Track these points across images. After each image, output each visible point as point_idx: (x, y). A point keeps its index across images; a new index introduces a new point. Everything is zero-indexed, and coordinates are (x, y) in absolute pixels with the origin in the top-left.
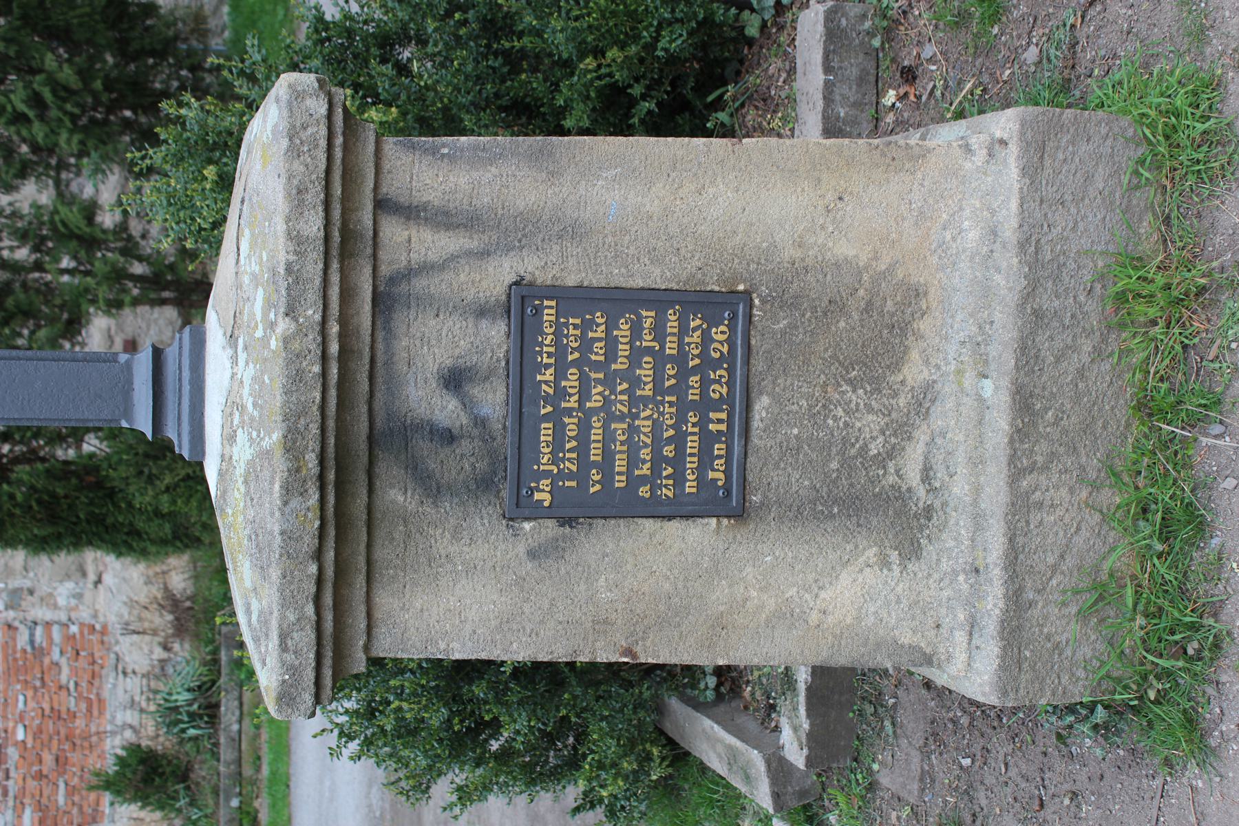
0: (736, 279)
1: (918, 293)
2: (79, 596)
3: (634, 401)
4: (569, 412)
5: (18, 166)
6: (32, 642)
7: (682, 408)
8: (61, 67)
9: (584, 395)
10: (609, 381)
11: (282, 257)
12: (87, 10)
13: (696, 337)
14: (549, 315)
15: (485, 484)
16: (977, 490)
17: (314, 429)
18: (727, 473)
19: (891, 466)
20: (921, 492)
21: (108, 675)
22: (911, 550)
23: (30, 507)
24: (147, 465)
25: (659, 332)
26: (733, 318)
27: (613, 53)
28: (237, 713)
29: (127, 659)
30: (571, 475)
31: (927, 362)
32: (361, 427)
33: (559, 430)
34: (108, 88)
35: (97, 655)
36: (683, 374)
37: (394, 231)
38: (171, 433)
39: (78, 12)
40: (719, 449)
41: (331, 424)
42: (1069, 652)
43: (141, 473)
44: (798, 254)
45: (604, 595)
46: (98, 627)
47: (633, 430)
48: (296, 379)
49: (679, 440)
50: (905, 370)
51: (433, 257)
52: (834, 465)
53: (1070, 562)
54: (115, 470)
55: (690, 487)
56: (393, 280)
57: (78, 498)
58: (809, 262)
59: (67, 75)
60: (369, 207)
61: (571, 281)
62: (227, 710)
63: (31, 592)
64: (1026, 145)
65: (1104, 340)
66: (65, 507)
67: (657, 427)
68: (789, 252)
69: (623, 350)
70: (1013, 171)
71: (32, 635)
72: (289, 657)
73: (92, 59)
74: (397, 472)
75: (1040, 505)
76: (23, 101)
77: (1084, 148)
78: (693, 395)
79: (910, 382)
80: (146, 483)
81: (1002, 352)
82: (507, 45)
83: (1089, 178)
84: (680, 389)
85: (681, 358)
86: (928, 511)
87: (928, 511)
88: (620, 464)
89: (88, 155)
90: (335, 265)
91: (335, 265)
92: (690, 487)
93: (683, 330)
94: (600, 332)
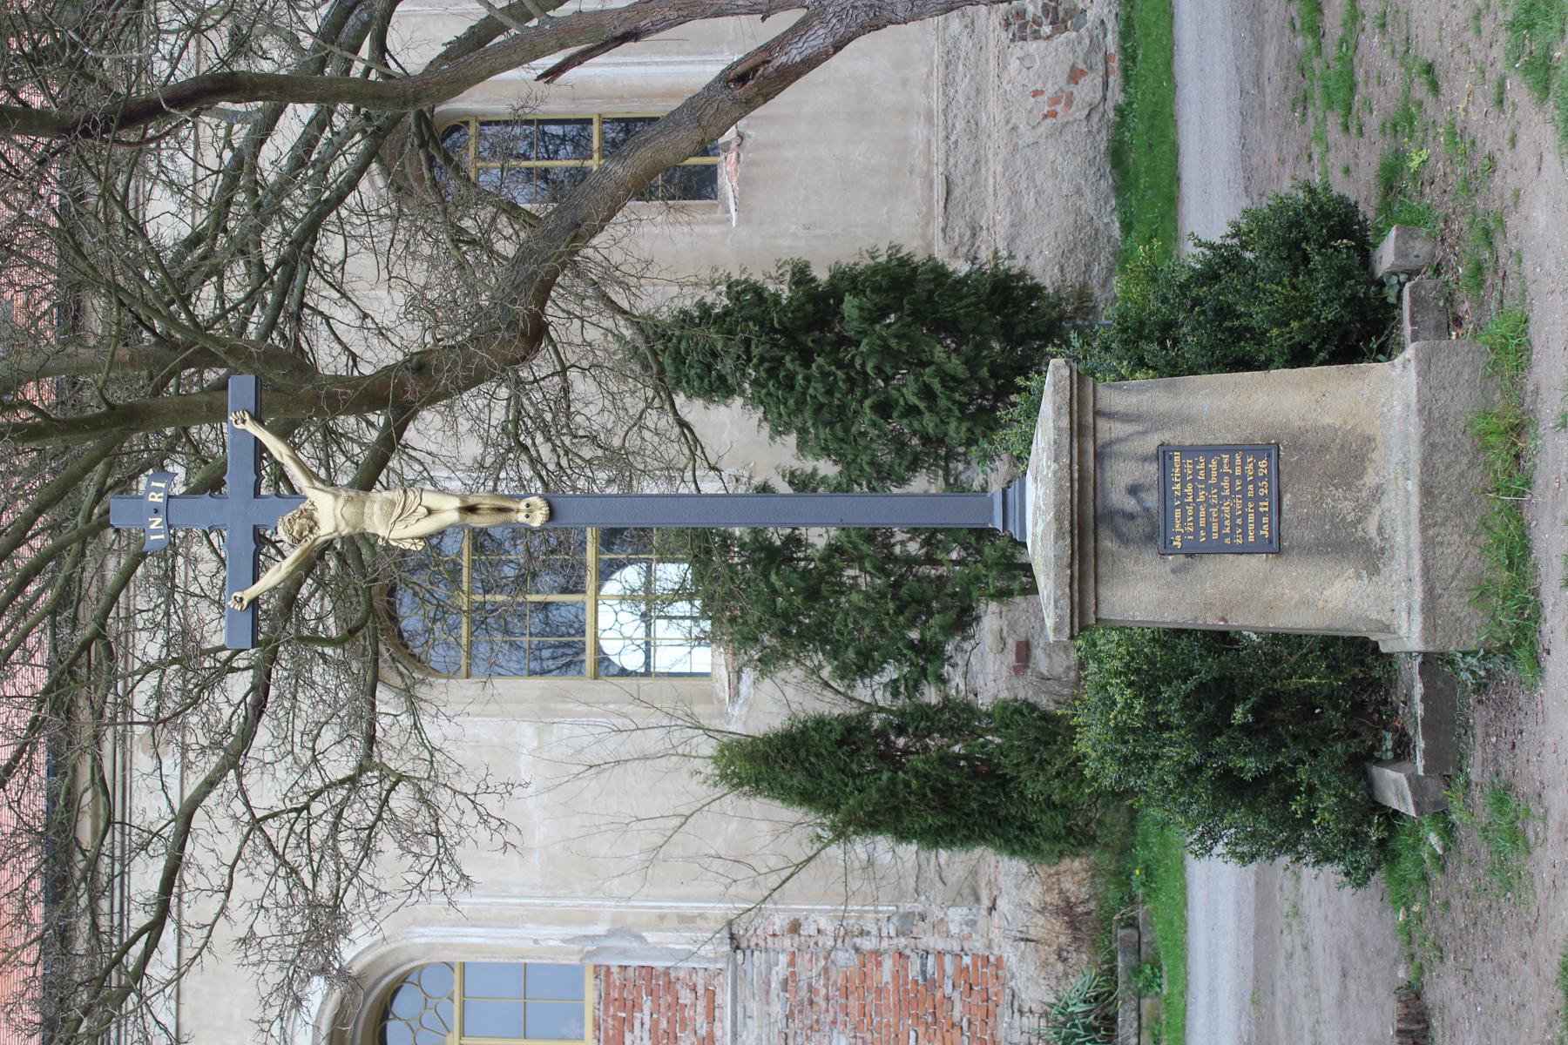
0: (1271, 437)
1: (1370, 439)
2: (972, 924)
3: (1220, 498)
4: (1188, 504)
5: (910, 458)
6: (924, 973)
7: (1245, 500)
8: (949, 358)
9: (1195, 495)
10: (1208, 489)
11: (1052, 437)
12: (973, 299)
13: (1251, 466)
14: (1177, 459)
15: (1150, 538)
16: (1408, 538)
17: (1068, 511)
18: (1270, 531)
19: (1360, 527)
20: (1378, 540)
21: (1003, 1015)
22: (1374, 571)
23: (925, 795)
24: (1038, 750)
25: (1232, 465)
26: (1269, 456)
27: (1294, 325)
28: (1135, 1025)
29: (1023, 996)
30: (1191, 534)
31: (1378, 474)
32: (1091, 512)
33: (1184, 512)
34: (994, 374)
35: (991, 991)
36: (1245, 484)
37: (1103, 424)
38: (1012, 530)
39: (964, 302)
40: (1265, 520)
41: (1075, 509)
42: (1466, 622)
43: (1032, 759)
44: (1302, 424)
45: (1209, 591)
46: (992, 959)
47: (1220, 512)
48: (1060, 488)
49: (1244, 516)
50: (1365, 479)
51: (1122, 435)
52: (1327, 527)
53: (1462, 574)
54: (1006, 757)
55: (1251, 539)
56: (1103, 446)
57: (970, 787)
58: (1308, 427)
59: (955, 365)
60: (1091, 414)
61: (1188, 443)
62: (1124, 1021)
63: (923, 919)
64: (1419, 361)
65: (1475, 457)
66: (958, 795)
67: (1232, 510)
68: (1297, 423)
69: (1214, 474)
70: (1414, 375)
71: (924, 965)
72: (1059, 611)
73: (979, 347)
74: (1108, 532)
75: (1442, 544)
76: (914, 394)
77: (1455, 359)
78: (1251, 494)
79: (1368, 484)
80: (1037, 769)
81: (1415, 467)
82: (1230, 324)
83: (1459, 374)
84: (1244, 491)
85: (1244, 476)
86: (1383, 550)
87: (1383, 550)
88: (1215, 528)
89: (976, 442)
90: (1075, 440)
91: (1075, 440)
92: (1251, 539)
93: (1244, 463)
94: (1202, 466)
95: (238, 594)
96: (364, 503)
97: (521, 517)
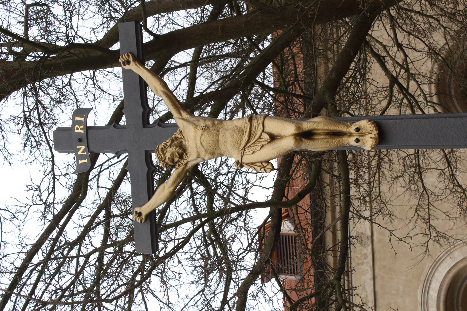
95: (137, 209)
96: (218, 131)
97: (352, 141)
